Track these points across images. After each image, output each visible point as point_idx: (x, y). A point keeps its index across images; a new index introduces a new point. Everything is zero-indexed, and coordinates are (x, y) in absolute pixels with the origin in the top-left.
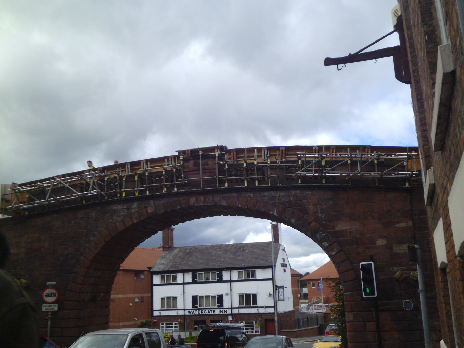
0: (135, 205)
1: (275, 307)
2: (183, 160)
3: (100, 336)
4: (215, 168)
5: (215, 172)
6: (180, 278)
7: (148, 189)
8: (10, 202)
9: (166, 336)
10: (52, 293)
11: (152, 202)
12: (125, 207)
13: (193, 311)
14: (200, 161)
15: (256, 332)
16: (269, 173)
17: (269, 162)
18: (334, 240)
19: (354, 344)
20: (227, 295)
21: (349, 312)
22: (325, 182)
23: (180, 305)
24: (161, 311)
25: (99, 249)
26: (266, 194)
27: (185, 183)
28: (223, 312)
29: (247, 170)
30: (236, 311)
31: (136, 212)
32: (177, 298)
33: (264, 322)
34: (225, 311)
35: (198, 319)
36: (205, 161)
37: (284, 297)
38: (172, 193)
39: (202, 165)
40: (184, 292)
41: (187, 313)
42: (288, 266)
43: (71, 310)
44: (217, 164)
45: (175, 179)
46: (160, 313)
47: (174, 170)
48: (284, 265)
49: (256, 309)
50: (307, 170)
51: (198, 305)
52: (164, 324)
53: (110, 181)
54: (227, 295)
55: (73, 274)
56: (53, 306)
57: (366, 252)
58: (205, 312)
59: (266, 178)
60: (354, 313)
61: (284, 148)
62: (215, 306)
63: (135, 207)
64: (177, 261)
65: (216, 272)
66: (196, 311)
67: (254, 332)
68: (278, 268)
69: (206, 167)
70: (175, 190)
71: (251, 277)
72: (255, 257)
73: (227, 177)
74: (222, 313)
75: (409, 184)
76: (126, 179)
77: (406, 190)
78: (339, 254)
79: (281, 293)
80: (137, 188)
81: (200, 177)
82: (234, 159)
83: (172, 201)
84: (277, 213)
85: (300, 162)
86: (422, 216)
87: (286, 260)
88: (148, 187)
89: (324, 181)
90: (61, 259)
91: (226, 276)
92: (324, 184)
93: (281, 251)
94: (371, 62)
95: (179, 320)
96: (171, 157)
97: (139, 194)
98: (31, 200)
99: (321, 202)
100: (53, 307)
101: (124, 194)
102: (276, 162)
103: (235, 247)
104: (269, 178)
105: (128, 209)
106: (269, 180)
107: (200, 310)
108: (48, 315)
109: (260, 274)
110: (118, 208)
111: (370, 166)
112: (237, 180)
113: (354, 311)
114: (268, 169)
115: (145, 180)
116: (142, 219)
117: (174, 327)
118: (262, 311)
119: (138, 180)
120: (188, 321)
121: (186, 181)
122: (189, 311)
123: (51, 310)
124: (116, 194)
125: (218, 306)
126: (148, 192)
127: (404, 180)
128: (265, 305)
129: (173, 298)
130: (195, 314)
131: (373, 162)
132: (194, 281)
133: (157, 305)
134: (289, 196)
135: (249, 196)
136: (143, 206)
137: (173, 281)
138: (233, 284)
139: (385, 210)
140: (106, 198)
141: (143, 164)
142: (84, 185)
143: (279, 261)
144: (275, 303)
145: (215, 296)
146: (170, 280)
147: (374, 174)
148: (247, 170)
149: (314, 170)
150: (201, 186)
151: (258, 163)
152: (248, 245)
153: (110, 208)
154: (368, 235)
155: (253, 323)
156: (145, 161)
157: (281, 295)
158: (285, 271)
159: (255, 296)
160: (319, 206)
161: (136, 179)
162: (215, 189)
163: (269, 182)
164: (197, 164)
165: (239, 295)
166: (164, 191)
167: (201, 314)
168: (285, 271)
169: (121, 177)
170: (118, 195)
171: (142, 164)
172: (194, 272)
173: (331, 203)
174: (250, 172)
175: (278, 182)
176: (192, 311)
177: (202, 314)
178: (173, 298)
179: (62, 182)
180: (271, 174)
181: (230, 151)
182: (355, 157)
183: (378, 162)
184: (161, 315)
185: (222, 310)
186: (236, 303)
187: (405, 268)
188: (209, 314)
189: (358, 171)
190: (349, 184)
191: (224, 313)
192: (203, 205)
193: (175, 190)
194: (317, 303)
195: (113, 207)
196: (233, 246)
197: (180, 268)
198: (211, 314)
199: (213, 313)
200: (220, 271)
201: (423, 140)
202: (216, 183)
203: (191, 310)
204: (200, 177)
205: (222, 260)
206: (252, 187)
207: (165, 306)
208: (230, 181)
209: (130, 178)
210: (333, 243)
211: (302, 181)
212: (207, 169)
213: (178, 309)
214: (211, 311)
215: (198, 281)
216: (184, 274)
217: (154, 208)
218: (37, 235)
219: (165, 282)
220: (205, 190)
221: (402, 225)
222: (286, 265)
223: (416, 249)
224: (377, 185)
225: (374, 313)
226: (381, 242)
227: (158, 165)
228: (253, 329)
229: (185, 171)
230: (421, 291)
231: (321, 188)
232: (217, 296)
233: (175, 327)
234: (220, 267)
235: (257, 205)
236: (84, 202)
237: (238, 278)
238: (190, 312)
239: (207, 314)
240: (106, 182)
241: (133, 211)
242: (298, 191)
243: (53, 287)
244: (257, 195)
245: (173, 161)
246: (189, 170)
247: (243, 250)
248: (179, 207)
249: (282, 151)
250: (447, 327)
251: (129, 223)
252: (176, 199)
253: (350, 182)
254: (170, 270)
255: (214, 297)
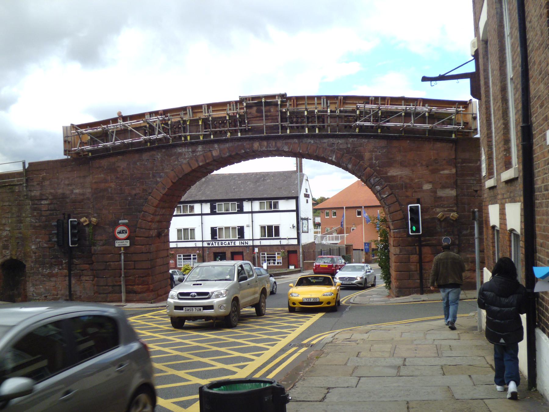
0: (200, 148)
1: (298, 238)
2: (247, 107)
3: (210, 267)
4: (277, 115)
5: (277, 119)
6: (197, 208)
7: (212, 134)
8: (71, 143)
9: (188, 268)
10: (123, 230)
11: (216, 146)
12: (190, 150)
13: (212, 243)
14: (264, 108)
15: (278, 263)
16: (329, 122)
17: (329, 111)
18: (386, 184)
19: (399, 273)
20: (248, 226)
21: (396, 246)
22: (381, 131)
23: (198, 237)
24: (178, 243)
25: (166, 189)
26: (325, 140)
27: (248, 129)
28: (243, 244)
29: (308, 118)
30: (257, 243)
31: (201, 154)
32: (194, 229)
33: (286, 253)
34: (246, 243)
35: (218, 251)
36: (268, 108)
37: (308, 229)
38: (237, 137)
39: (265, 112)
40: (202, 223)
41: (205, 245)
42: (310, 196)
43: (143, 245)
44: (279, 112)
45: (238, 125)
46: (177, 245)
47: (238, 116)
48: (307, 196)
49: (279, 241)
50: (365, 121)
51: (218, 237)
52: (191, 255)
53: (173, 125)
54: (248, 226)
55: (143, 213)
56: (125, 242)
57: (414, 195)
58: (225, 244)
59: (326, 126)
60: (400, 247)
61: (342, 98)
62: (236, 238)
63: (200, 150)
64: (193, 191)
65: (236, 203)
66: (215, 243)
67: (277, 263)
68: (302, 199)
69: (269, 114)
70: (239, 135)
71: (274, 208)
72: (278, 187)
73: (288, 124)
74: (243, 245)
75: (456, 136)
76: (190, 123)
77: (453, 141)
78: (390, 196)
79: (304, 225)
80: (202, 132)
81: (263, 123)
82: (294, 107)
83: (236, 145)
84: (335, 159)
85: (358, 112)
86: (464, 165)
87: (309, 191)
88: (212, 131)
89: (379, 131)
90: (129, 199)
91: (247, 206)
92: (379, 133)
93: (304, 181)
94: (454, 81)
95: (198, 252)
96: (232, 102)
97: (203, 138)
98: (93, 142)
99: (376, 150)
100: (125, 243)
101: (189, 138)
102: (336, 111)
103: (255, 176)
104: (328, 126)
105: (193, 152)
106: (329, 128)
107: (220, 242)
108: (121, 250)
109: (283, 205)
110: (183, 150)
111: (421, 118)
112: (298, 127)
113: (401, 245)
114: (328, 117)
115: (209, 125)
116: (207, 161)
117: (192, 259)
118: (284, 242)
119: (202, 125)
120: (207, 252)
121: (249, 126)
122: (208, 242)
123: (124, 246)
124: (180, 137)
125: (239, 238)
126: (212, 137)
127: (450, 132)
128: (288, 237)
129: (190, 229)
130: (214, 246)
131: (425, 114)
132: (213, 212)
133: (173, 236)
134: (347, 143)
135: (310, 142)
136: (208, 149)
137: (190, 212)
138: (255, 215)
139: (433, 158)
140: (171, 141)
141: (205, 108)
142: (148, 128)
143: (303, 192)
144: (298, 234)
145: (236, 228)
146: (187, 210)
147: (427, 126)
148: (308, 118)
149: (372, 121)
150: (265, 132)
151: (319, 111)
152: (269, 175)
153: (175, 150)
154: (416, 180)
155: (275, 254)
156: (206, 106)
157: (305, 227)
158: (307, 202)
159: (277, 228)
160: (374, 153)
161: (200, 123)
162: (278, 135)
163: (329, 130)
164: (260, 111)
165: (261, 227)
166: (228, 136)
167: (220, 245)
168: (307, 202)
169: (185, 122)
170: (183, 139)
171: (203, 108)
172: (213, 203)
173: (385, 151)
174: (310, 120)
175: (337, 130)
176: (211, 242)
177: (222, 245)
178: (190, 229)
179: (126, 125)
180: (331, 122)
181: (290, 98)
182: (409, 109)
183: (429, 114)
184: (178, 247)
185: (243, 241)
186: (258, 235)
187: (446, 209)
188: (229, 245)
189: (411, 124)
190: (402, 134)
191: (245, 245)
192: (266, 150)
193: (239, 135)
194: (331, 233)
195: (178, 150)
196: (253, 175)
197: (197, 198)
198: (231, 245)
199: (233, 245)
200: (240, 202)
201: (488, 147)
202: (279, 130)
203: (209, 242)
204: (263, 124)
205: (243, 190)
206: (312, 134)
207: (182, 237)
208: (291, 128)
209: (194, 122)
210: (385, 187)
211: (359, 130)
212: (269, 116)
213: (196, 240)
214: (232, 242)
215: (217, 212)
216: (201, 205)
217: (218, 152)
218: (102, 176)
219: (181, 213)
220: (268, 136)
221: (446, 172)
222: (309, 195)
223: (476, 212)
224: (427, 135)
225: (417, 248)
226: (427, 187)
227: (221, 109)
228: (275, 260)
229: (248, 117)
230: (477, 238)
231: (376, 137)
232: (237, 228)
233: (194, 259)
234: (241, 198)
235: (317, 151)
236: (149, 144)
237: (260, 209)
238: (209, 244)
239: (227, 245)
240: (169, 125)
241: (198, 154)
242: (355, 139)
243: (124, 225)
244: (317, 142)
245: (235, 106)
246: (252, 117)
247: (264, 180)
248: (243, 151)
249: (341, 100)
250: (492, 260)
251: (195, 166)
252: (240, 143)
253: (403, 133)
254: (186, 200)
255: (234, 228)
